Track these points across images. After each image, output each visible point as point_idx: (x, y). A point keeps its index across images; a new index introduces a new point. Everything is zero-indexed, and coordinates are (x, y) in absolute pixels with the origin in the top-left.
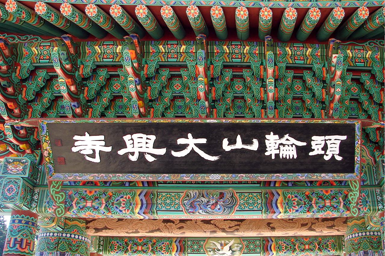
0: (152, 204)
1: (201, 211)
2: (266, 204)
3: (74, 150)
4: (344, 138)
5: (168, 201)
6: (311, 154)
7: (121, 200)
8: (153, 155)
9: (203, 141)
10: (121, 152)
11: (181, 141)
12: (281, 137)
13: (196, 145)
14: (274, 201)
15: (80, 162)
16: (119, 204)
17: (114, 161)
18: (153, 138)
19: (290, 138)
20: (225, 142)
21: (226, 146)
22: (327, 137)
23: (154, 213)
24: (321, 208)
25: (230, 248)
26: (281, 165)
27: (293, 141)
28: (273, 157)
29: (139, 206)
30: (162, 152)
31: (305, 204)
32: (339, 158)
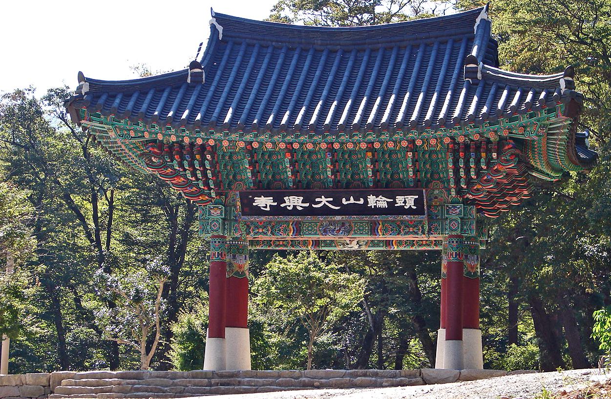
0: (300, 230)
1: (330, 234)
2: (371, 230)
3: (254, 204)
4: (417, 197)
5: (310, 228)
6: (396, 205)
7: (281, 228)
8: (301, 207)
9: (331, 199)
10: (282, 205)
11: (317, 200)
12: (377, 197)
13: (327, 201)
14: (376, 228)
15: (258, 211)
16: (280, 230)
17: (277, 211)
18: (302, 198)
19: (382, 197)
20: (344, 200)
21: (344, 202)
22: (405, 197)
23: (301, 235)
24: (406, 233)
25: (358, 243)
26: (377, 211)
27: (384, 199)
28: (373, 207)
29: (292, 231)
30: (307, 205)
31: (396, 230)
32: (415, 208)
